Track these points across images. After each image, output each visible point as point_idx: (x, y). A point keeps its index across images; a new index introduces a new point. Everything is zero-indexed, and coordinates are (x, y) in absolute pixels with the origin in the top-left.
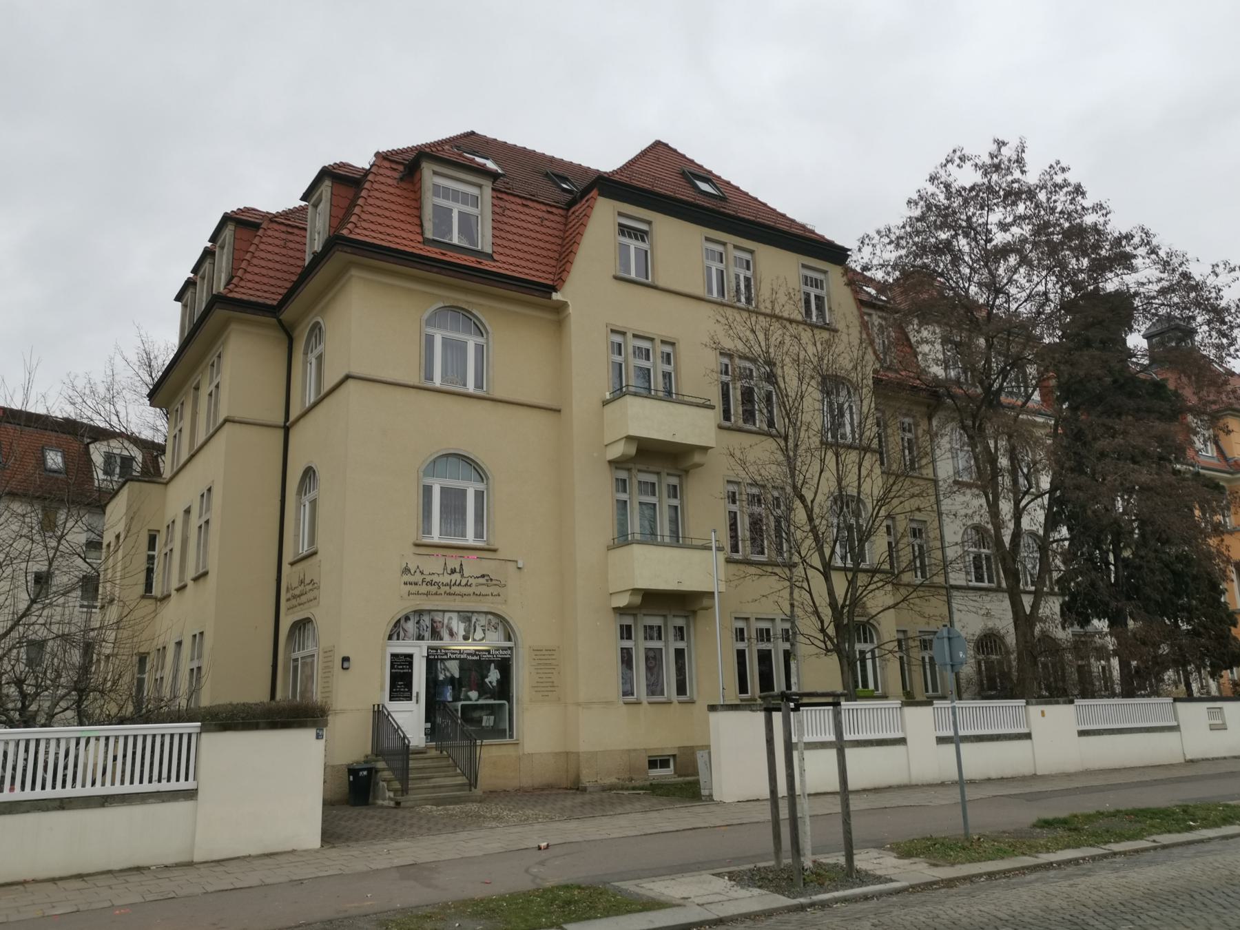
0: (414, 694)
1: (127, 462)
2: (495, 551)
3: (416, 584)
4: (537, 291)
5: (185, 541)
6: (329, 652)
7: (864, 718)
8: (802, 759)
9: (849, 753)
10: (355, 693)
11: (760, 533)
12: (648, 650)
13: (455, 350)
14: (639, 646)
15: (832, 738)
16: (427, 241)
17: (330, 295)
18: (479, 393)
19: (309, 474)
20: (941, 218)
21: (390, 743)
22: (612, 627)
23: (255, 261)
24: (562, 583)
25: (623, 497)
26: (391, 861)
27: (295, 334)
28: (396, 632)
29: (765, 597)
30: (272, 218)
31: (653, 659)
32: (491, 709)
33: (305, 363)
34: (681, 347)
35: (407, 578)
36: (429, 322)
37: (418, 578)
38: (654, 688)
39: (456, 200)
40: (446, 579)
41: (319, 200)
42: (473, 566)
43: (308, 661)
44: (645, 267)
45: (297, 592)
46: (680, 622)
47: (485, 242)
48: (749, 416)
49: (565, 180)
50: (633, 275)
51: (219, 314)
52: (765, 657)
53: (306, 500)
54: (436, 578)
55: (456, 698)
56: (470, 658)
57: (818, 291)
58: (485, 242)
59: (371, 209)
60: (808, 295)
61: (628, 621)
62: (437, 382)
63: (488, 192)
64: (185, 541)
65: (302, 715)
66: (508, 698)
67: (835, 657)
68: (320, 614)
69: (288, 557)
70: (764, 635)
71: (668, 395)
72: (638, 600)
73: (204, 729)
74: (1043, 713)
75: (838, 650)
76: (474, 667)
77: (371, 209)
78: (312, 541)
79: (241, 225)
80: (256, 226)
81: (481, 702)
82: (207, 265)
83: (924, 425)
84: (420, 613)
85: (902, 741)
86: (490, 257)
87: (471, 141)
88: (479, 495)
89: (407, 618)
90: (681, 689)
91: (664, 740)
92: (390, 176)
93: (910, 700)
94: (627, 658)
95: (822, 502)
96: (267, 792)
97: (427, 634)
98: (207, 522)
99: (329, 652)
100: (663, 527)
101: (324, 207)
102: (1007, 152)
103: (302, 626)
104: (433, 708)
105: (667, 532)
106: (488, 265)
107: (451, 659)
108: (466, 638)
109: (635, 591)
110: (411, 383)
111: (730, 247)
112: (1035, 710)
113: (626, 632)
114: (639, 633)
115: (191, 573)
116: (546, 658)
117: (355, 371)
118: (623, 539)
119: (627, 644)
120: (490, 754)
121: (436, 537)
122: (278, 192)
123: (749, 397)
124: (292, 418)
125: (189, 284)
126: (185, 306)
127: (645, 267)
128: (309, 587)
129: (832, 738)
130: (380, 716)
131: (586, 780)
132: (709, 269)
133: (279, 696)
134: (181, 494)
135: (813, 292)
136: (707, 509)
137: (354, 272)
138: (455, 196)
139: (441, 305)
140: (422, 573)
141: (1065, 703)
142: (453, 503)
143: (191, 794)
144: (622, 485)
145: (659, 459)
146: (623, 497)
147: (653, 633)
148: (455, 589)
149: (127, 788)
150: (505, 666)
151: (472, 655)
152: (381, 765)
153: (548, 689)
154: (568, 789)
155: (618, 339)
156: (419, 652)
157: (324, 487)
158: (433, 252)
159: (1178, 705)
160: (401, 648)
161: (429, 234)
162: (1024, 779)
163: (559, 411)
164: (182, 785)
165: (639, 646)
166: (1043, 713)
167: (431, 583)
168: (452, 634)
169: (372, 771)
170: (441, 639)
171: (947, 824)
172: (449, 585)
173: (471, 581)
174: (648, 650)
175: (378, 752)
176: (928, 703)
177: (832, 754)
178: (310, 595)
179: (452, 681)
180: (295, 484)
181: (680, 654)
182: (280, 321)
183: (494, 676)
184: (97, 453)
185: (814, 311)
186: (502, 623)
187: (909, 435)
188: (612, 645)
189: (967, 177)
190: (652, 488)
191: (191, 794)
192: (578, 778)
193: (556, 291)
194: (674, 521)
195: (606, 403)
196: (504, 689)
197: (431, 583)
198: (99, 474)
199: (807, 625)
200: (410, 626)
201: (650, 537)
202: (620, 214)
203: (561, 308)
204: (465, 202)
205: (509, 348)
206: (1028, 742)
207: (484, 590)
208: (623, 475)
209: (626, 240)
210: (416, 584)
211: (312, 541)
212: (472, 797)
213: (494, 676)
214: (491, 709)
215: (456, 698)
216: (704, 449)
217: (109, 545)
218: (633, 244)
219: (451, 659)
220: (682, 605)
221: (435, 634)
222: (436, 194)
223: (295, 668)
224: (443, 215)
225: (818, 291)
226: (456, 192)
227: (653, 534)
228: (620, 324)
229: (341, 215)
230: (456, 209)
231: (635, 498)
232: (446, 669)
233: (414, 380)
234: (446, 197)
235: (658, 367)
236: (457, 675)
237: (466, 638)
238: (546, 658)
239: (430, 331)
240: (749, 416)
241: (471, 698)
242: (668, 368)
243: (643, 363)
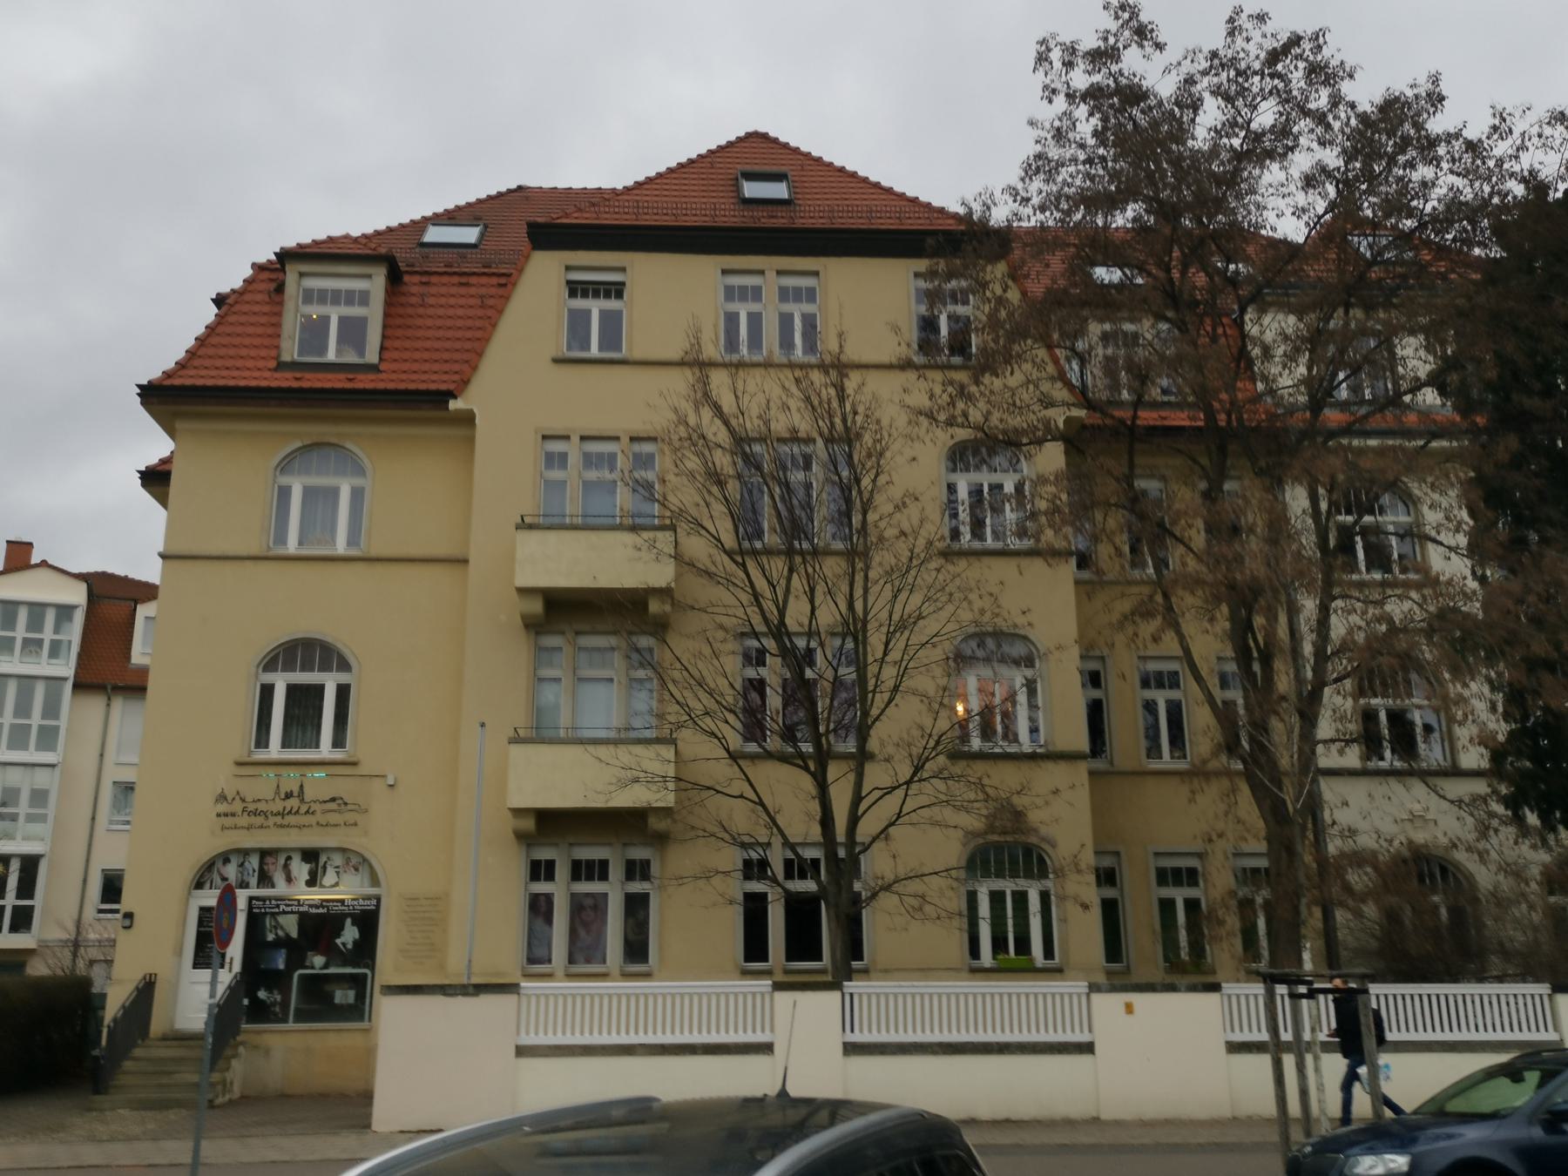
0: (227, 960)
2: (354, 764)
3: (233, 815)
4: (416, 401)
8: (1317, 1070)
9: (1265, 1060)
15: (1264, 1036)
16: (282, 366)
18: (354, 552)
22: (515, 866)
31: (586, 913)
35: (223, 808)
37: (237, 806)
40: (278, 806)
54: (262, 806)
56: (314, 911)
74: (1129, 1008)
76: (319, 927)
81: (332, 970)
84: (245, 853)
85: (1087, 1048)
89: (225, 858)
93: (1119, 969)
94: (540, 908)
97: (254, 881)
107: (284, 912)
110: (243, 552)
111: (771, 275)
119: (542, 887)
127: (612, 336)
129: (1264, 1036)
138: (336, 297)
139: (298, 444)
140: (243, 800)
141: (1193, 988)
147: (580, 870)
148: (290, 819)
150: (368, 921)
151: (317, 907)
158: (285, 380)
159: (1095, 997)
162: (1069, 1123)
163: (465, 561)
166: (1129, 1008)
167: (255, 813)
168: (289, 880)
170: (273, 886)
172: (282, 814)
173: (315, 807)
177: (1265, 1060)
179: (284, 942)
183: (350, 934)
186: (358, 862)
193: (455, 397)
196: (366, 949)
197: (255, 813)
202: (568, 268)
203: (468, 419)
205: (388, 486)
207: (334, 818)
209: (579, 303)
210: (233, 815)
213: (350, 934)
219: (284, 912)
224: (315, 332)
228: (557, 427)
232: (277, 926)
236: (294, 934)
237: (312, 882)
238: (430, 913)
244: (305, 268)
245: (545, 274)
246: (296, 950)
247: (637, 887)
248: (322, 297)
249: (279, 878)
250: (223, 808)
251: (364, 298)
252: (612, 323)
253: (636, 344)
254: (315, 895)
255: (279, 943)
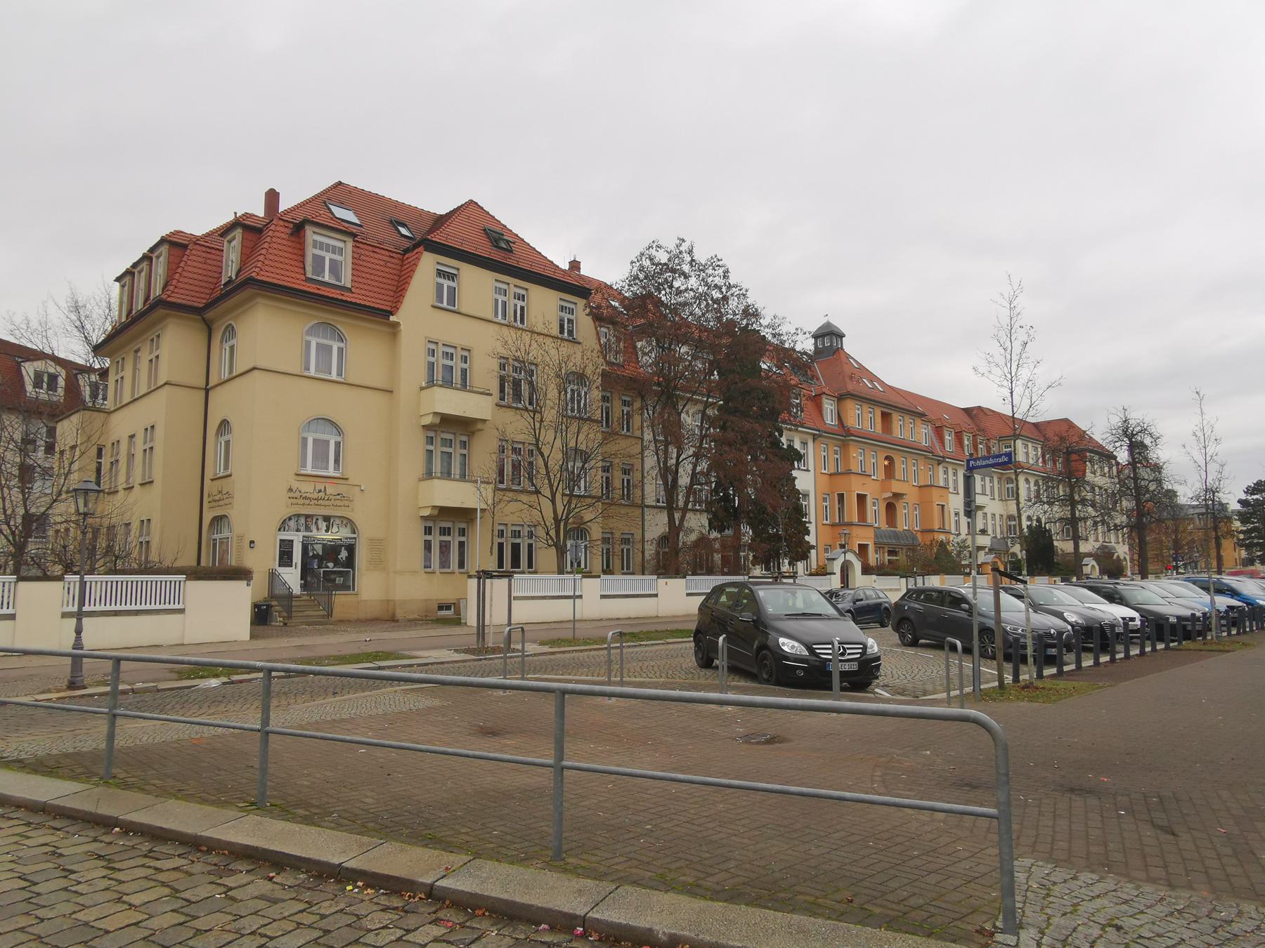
1: (53, 378)
4: (379, 314)
5: (131, 456)
6: (241, 538)
7: (523, 583)
9: (85, 620)
10: (262, 559)
11: (516, 470)
12: (441, 542)
13: (324, 350)
14: (436, 539)
16: (308, 280)
17: (246, 307)
19: (224, 425)
20: (657, 273)
21: (279, 591)
23: (185, 274)
24: (388, 498)
25: (431, 448)
26: (282, 648)
27: (215, 326)
28: (283, 527)
29: (516, 512)
30: (196, 241)
31: (445, 547)
32: (340, 574)
33: (221, 349)
34: (475, 353)
35: (291, 495)
36: (309, 332)
37: (297, 495)
38: (444, 563)
39: (328, 251)
40: (315, 495)
41: (234, 238)
42: (331, 490)
43: (225, 542)
44: (452, 300)
45: (217, 498)
46: (463, 525)
47: (346, 280)
48: (517, 396)
49: (404, 225)
50: (445, 305)
51: (161, 312)
52: (516, 548)
53: (222, 440)
55: (320, 567)
57: (570, 317)
58: (346, 280)
59: (271, 257)
60: (562, 320)
61: (430, 524)
62: (312, 372)
63: (350, 243)
64: (131, 456)
65: (241, 574)
66: (353, 568)
67: (553, 550)
68: (234, 514)
69: (209, 474)
70: (516, 534)
71: (464, 386)
72: (436, 512)
73: (187, 579)
75: (556, 545)
76: (331, 551)
77: (271, 257)
78: (226, 468)
79: (176, 245)
80: (185, 247)
82: (145, 265)
83: (637, 405)
84: (299, 516)
85: (656, 595)
86: (349, 290)
87: (339, 193)
88: (338, 444)
89: (290, 519)
90: (461, 565)
91: (447, 595)
92: (279, 234)
94: (428, 546)
95: (556, 458)
96: (216, 616)
97: (302, 528)
98: (151, 448)
99: (241, 538)
100: (456, 470)
101: (237, 243)
102: (684, 247)
103: (218, 520)
104: (306, 571)
105: (458, 472)
106: (348, 297)
108: (327, 531)
109: (434, 507)
112: (662, 581)
113: (428, 531)
114: (436, 531)
115: (137, 478)
116: (378, 545)
117: (259, 365)
118: (429, 475)
119: (428, 538)
120: (341, 600)
121: (309, 470)
122: (200, 225)
123: (516, 385)
124: (211, 385)
125: (129, 273)
126: (123, 286)
127: (452, 300)
128: (225, 497)
130: (273, 575)
131: (400, 614)
132: (497, 301)
133: (203, 563)
134: (123, 425)
135: (566, 316)
136: (484, 454)
137: (260, 300)
138: (327, 248)
142: (321, 445)
143: (182, 611)
144: (430, 440)
145: (455, 428)
146: (431, 448)
147: (445, 531)
149: (148, 607)
150: (351, 549)
152: (274, 603)
153: (378, 563)
154: (389, 618)
155: (433, 346)
156: (297, 539)
157: (237, 436)
160: (286, 536)
161: (309, 275)
164: (176, 606)
165: (436, 539)
167: (305, 498)
169: (269, 607)
171: (569, 635)
172: (317, 499)
174: (441, 542)
175: (272, 596)
176: (60, 578)
178: (226, 501)
180: (214, 431)
181: (462, 544)
182: (204, 320)
183: (344, 554)
184: (29, 369)
185: (566, 333)
186: (350, 523)
187: (626, 409)
188: (420, 538)
189: (662, 257)
190: (449, 443)
191: (182, 611)
192: (394, 615)
194: (463, 465)
195: (422, 389)
196: (350, 562)
198: (29, 387)
199: (541, 532)
200: (292, 523)
201: (447, 475)
203: (396, 325)
204: (334, 252)
205: (361, 350)
206: (9, 623)
207: (339, 503)
208: (432, 434)
209: (441, 280)
211: (226, 468)
212: (328, 620)
213: (344, 554)
214: (340, 574)
215: (320, 567)
216: (484, 421)
217: (62, 453)
218: (446, 283)
220: (466, 515)
221: (308, 529)
222: (315, 247)
223: (215, 545)
224: (319, 261)
225: (570, 317)
226: (328, 245)
227: (449, 474)
228: (434, 337)
229: (247, 255)
230: (328, 256)
231: (438, 449)
233: (297, 371)
234: (321, 249)
235: (458, 365)
237: (327, 531)
238: (378, 545)
239: (309, 338)
240: (517, 396)
241: (330, 567)
242: (465, 366)
243: (449, 363)
244: (317, 230)
245: (428, 263)
246: (321, 559)
247: (462, 539)
248: (322, 246)
249: (314, 528)
250: (291, 495)
251: (341, 251)
252: (452, 291)
253: (465, 305)
254: (329, 536)
255: (315, 556)
